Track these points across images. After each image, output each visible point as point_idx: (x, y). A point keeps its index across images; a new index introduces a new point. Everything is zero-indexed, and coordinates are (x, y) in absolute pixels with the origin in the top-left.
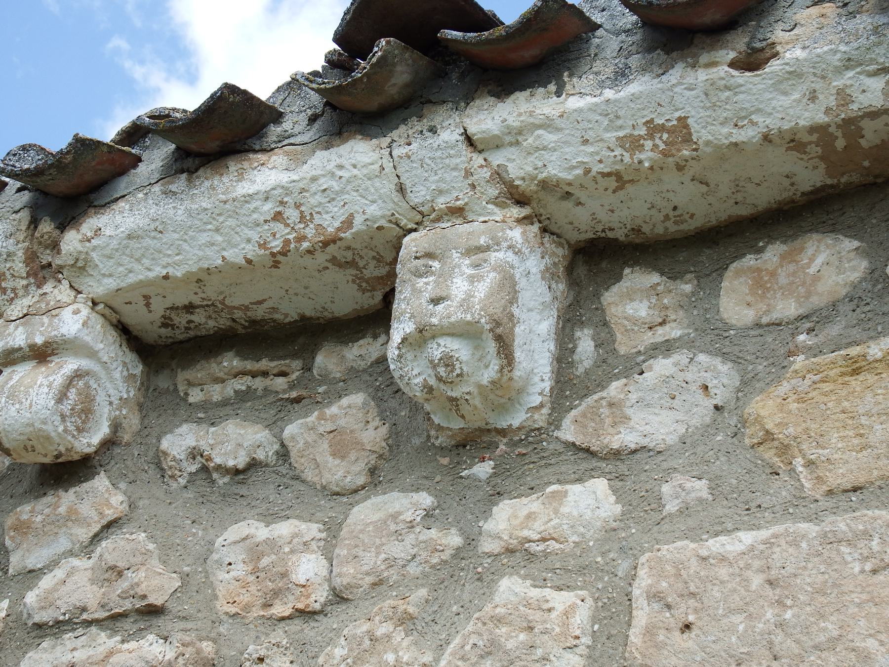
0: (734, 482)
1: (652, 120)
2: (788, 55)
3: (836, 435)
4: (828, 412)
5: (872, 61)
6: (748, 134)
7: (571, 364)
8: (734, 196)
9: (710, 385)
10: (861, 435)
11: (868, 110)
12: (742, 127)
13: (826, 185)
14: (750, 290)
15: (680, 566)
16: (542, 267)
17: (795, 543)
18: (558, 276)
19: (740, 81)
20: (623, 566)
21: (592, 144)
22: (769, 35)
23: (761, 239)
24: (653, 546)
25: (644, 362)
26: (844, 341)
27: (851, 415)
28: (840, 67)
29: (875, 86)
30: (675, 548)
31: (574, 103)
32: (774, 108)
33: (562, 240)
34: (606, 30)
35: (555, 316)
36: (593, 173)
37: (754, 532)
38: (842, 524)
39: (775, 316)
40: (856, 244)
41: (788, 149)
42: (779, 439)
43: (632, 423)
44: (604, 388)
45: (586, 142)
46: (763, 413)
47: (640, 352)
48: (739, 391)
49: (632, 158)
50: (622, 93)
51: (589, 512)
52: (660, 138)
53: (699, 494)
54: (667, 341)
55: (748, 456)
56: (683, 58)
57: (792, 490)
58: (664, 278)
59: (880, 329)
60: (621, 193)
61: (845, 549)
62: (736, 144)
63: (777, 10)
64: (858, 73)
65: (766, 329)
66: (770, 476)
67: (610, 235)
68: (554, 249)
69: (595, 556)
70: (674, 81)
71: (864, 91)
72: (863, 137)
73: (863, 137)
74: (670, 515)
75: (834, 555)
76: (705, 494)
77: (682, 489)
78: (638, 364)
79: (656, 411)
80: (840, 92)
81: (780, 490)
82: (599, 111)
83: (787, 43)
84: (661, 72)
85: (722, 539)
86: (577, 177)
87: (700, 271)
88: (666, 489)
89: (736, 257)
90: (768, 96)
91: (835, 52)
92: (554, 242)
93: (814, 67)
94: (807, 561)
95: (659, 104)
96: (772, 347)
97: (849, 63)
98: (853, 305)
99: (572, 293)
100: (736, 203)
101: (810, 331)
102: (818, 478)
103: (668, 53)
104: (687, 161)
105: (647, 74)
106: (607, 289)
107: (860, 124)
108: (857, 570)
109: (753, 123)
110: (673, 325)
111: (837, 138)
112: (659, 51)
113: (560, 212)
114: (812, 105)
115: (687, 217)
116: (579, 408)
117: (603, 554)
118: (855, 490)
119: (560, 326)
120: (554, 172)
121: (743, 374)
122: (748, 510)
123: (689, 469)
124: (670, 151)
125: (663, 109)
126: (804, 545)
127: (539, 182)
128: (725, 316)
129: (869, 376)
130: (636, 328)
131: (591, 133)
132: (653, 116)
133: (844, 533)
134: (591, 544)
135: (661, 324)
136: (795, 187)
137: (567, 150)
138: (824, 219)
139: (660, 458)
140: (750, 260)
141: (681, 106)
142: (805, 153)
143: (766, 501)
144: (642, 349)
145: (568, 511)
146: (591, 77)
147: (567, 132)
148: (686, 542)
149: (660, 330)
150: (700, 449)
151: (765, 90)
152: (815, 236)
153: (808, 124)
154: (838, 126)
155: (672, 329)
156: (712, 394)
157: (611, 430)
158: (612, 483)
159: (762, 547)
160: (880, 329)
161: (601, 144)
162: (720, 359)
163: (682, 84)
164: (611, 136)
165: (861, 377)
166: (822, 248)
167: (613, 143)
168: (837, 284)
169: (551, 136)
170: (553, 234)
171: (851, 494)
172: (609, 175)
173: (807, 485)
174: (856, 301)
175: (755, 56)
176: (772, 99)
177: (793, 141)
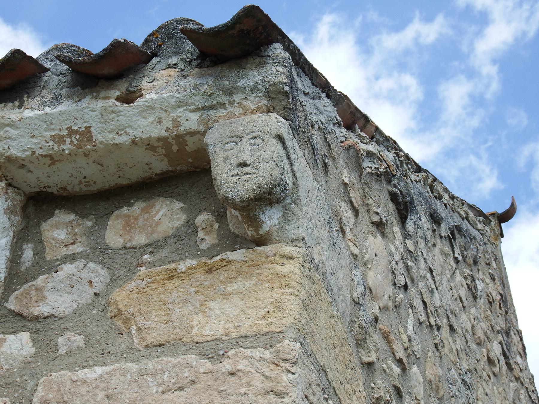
0: (98, 337)
1: (71, 126)
2: (147, 96)
3: (155, 314)
4: (153, 300)
5: (192, 104)
6: (123, 139)
7: (19, 264)
8: (118, 173)
9: (93, 281)
10: (168, 315)
11: (189, 131)
12: (121, 135)
13: (169, 170)
14: (123, 227)
15: (60, 385)
16: (5, 206)
17: (124, 375)
18: (16, 212)
19: (121, 109)
20: (31, 384)
21: (36, 138)
22: (139, 84)
23: (132, 198)
24: (48, 373)
25: (59, 265)
26: (168, 260)
27: (164, 303)
28: (175, 105)
29: (193, 118)
30: (60, 375)
31: (28, 113)
32: (138, 126)
33: (20, 191)
34: (52, 72)
35: (12, 236)
36: (37, 154)
37: (103, 368)
38: (150, 365)
39: (134, 243)
40: (182, 205)
41: (146, 149)
42: (125, 314)
43: (47, 301)
44: (35, 279)
45: (33, 136)
46: (118, 299)
47: (58, 259)
48: (109, 285)
49: (59, 148)
50: (55, 110)
51: (16, 351)
52: (75, 137)
53: (78, 344)
54: (74, 254)
55: (108, 323)
56: (91, 93)
57: (128, 344)
58: (77, 217)
59: (187, 254)
60: (53, 167)
61: (149, 379)
62: (117, 144)
63: (146, 70)
64: (184, 110)
65: (128, 250)
66: (118, 335)
67: (49, 190)
68: (15, 197)
69: (16, 378)
70: (84, 106)
71: (187, 120)
72: (187, 145)
73: (187, 145)
74: (61, 355)
75: (143, 382)
76: (81, 344)
77: (70, 340)
78: (56, 266)
79: (62, 294)
80: (174, 120)
81: (122, 343)
82: (41, 119)
83: (148, 90)
84: (78, 100)
85: (86, 370)
86: (27, 156)
87: (97, 214)
88: (60, 340)
89: (118, 208)
90: (135, 118)
91: (173, 97)
92: (15, 192)
93: (161, 105)
94: (129, 385)
95: (75, 118)
96: (130, 261)
97: (180, 104)
98: (175, 240)
99: (24, 222)
100: (119, 177)
101: (151, 253)
102: (142, 338)
103: (83, 89)
104: (90, 152)
105: (70, 100)
106: (44, 221)
107: (185, 138)
108: (154, 391)
109: (127, 133)
110: (79, 244)
111: (173, 145)
112: (79, 87)
113: (19, 175)
114: (159, 126)
115: (92, 183)
116: (20, 290)
117: (21, 377)
118: (160, 345)
119: (15, 241)
120: (14, 152)
121: (112, 275)
122: (103, 354)
123: (75, 329)
124: (80, 145)
125: (77, 121)
126: (129, 376)
127: (6, 157)
128: (107, 241)
129: (177, 281)
130: (58, 245)
131: (36, 132)
132: (71, 125)
133: (151, 370)
134: (15, 370)
135: (72, 244)
136: (152, 170)
137: (22, 140)
138: (167, 190)
139: (61, 322)
140: (125, 210)
141: (87, 120)
142: (156, 152)
143: (113, 349)
144: (59, 258)
145: (5, 350)
146: (39, 99)
147: (23, 130)
148: (66, 371)
149: (71, 247)
150: (83, 317)
151: (134, 115)
152: (161, 199)
153: (156, 136)
154: (173, 139)
155: (78, 247)
156: (94, 286)
157: (35, 304)
158: (32, 335)
159: (106, 376)
160: (187, 254)
161: (42, 138)
162: (101, 266)
163: (89, 108)
164: (48, 134)
165: (173, 282)
166: (164, 206)
167: (48, 138)
168: (169, 227)
169: (13, 131)
170: (15, 187)
171: (158, 348)
172: (46, 156)
173: (136, 341)
174: (177, 238)
175: (130, 95)
176: (137, 120)
177: (148, 145)
